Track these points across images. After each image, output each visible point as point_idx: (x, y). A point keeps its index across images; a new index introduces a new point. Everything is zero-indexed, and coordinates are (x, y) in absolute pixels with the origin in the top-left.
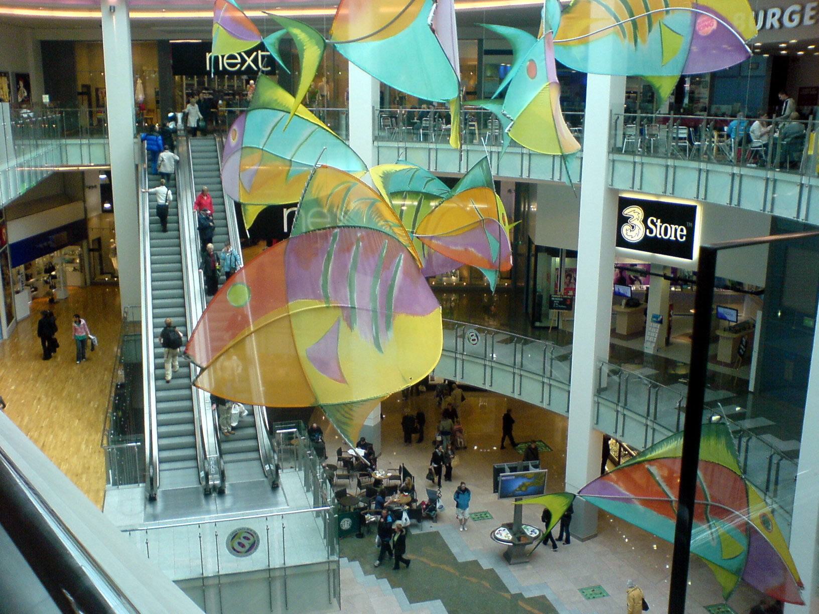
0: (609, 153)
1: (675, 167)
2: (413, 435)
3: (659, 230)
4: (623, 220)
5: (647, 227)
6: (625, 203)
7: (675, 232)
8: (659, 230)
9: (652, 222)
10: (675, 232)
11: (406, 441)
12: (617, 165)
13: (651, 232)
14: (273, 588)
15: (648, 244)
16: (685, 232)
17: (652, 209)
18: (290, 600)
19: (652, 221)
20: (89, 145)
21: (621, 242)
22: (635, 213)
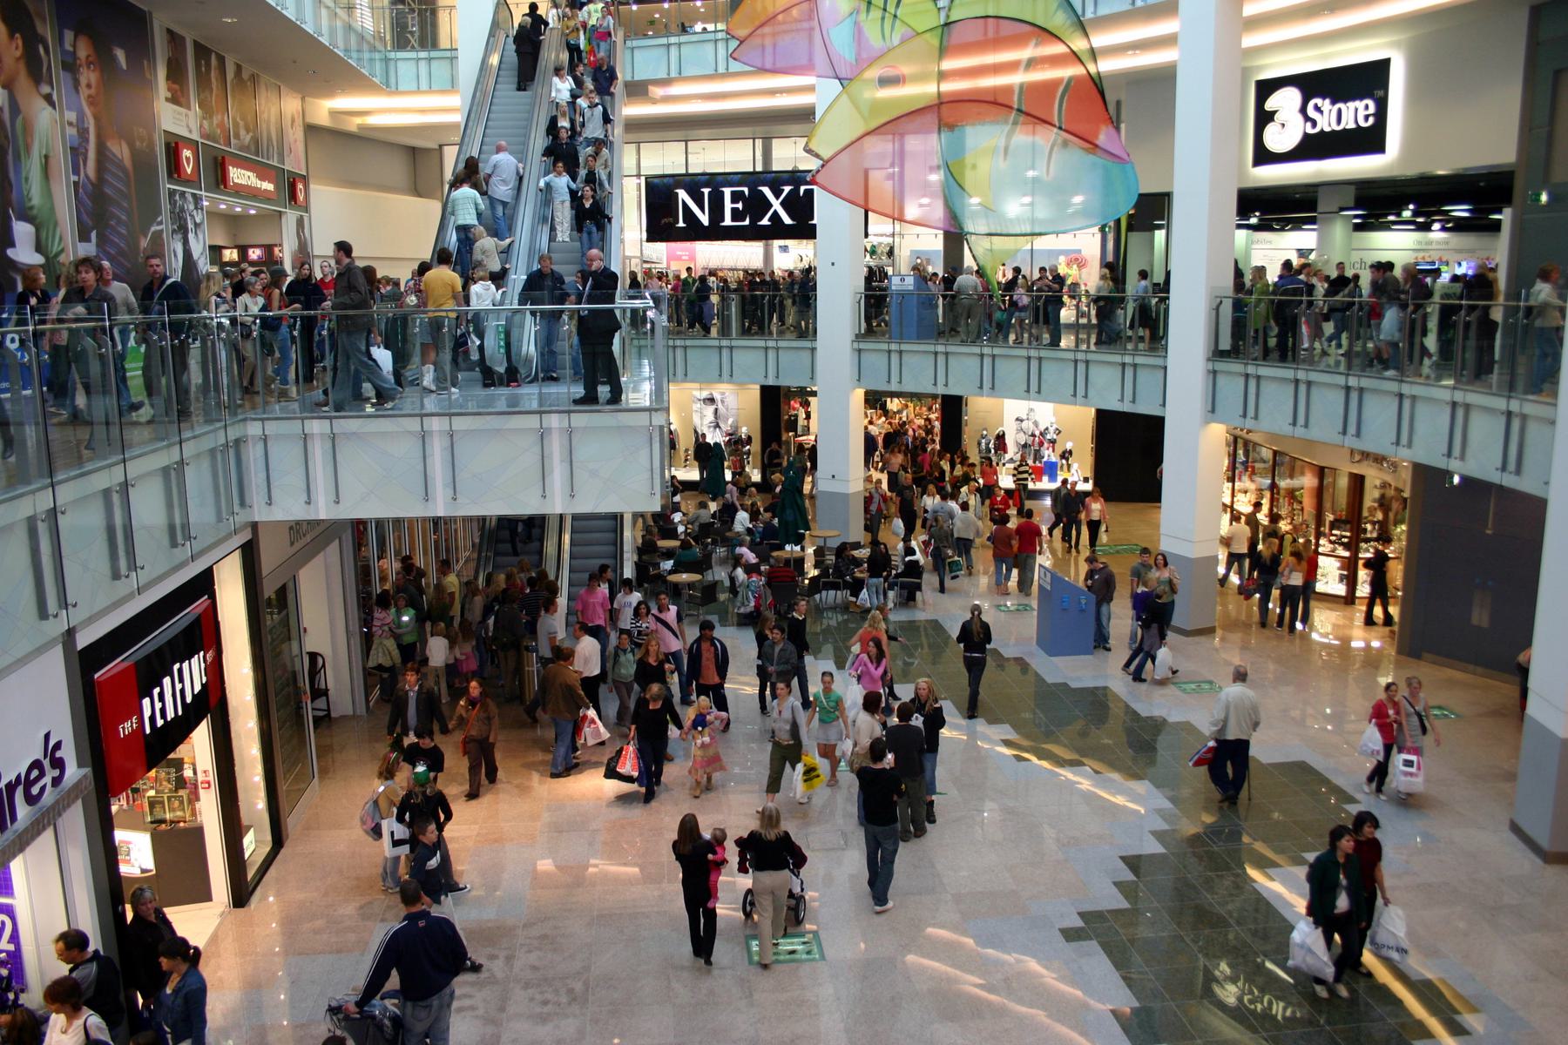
0: (1208, 360)
1: (1309, 384)
2: (816, 572)
3: (1332, 116)
4: (1264, 118)
5: (1307, 118)
6: (1266, 88)
7: (1356, 113)
8: (1332, 116)
9: (1317, 108)
10: (1356, 113)
11: (768, 791)
12: (1221, 380)
13: (1314, 124)
14: (244, 457)
15: (1314, 146)
16: (1372, 110)
17: (1314, 85)
18: (275, 493)
19: (1317, 108)
20: (430, 59)
21: (1263, 156)
22: (1286, 101)
